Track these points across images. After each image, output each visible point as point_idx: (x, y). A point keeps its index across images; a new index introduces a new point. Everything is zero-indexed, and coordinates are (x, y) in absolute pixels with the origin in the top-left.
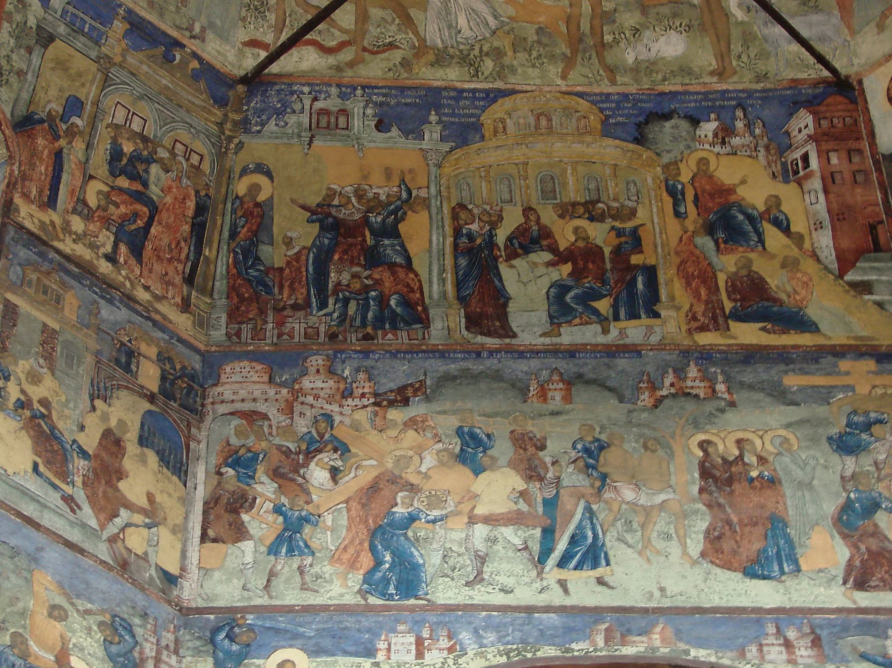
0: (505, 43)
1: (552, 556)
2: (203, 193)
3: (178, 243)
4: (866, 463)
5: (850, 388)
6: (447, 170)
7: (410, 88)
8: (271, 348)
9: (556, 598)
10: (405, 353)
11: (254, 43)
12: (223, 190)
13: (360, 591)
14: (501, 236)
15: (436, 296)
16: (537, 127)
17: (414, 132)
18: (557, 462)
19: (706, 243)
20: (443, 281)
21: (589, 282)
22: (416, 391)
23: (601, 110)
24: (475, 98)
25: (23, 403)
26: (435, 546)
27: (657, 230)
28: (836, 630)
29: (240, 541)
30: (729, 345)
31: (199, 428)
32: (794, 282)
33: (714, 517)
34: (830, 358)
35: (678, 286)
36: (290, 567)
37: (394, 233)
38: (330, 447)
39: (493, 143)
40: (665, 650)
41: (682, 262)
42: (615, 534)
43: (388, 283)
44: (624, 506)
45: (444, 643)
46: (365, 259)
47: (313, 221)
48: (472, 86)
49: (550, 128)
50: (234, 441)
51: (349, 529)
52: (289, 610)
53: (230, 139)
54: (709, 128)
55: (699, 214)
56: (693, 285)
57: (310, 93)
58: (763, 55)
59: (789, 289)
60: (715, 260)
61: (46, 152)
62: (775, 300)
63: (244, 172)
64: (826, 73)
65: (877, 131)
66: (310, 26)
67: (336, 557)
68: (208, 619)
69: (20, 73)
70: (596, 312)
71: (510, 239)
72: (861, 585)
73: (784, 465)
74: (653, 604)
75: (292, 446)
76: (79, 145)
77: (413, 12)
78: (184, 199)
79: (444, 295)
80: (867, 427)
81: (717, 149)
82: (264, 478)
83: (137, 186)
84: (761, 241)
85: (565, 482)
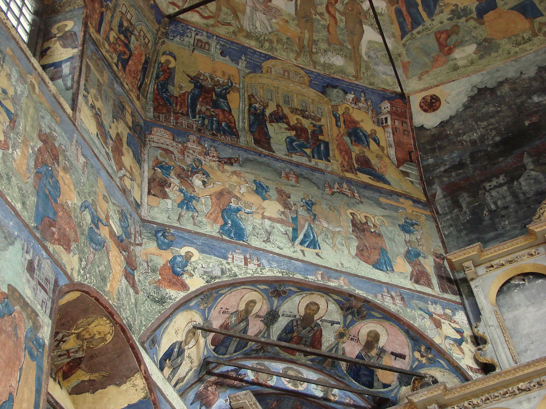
0: (274, 39)
1: (297, 240)
2: (147, 56)
3: (137, 72)
4: (413, 238)
5: (404, 209)
6: (247, 80)
7: (235, 43)
8: (173, 127)
9: (300, 256)
10: (230, 145)
12: (155, 58)
13: (219, 232)
14: (268, 112)
15: (241, 128)
16: (284, 75)
18: (295, 204)
19: (347, 139)
20: (244, 123)
21: (302, 141)
22: (236, 161)
23: (310, 77)
24: (260, 56)
25: (93, 106)
26: (249, 223)
27: (329, 129)
28: (409, 296)
29: (165, 198)
30: (358, 180)
31: (144, 149)
32: (381, 164)
33: (359, 242)
34: (396, 196)
35: (337, 153)
36: (188, 214)
38: (201, 172)
39: (265, 76)
40: (345, 287)
41: (339, 144)
42: (322, 238)
44: (324, 228)
45: (256, 262)
46: (212, 104)
47: (191, 82)
48: (260, 51)
49: (289, 77)
50: (159, 158)
51: (212, 206)
52: (189, 232)
53: (160, 38)
54: (351, 96)
55: (345, 128)
56: (343, 154)
57: (195, 31)
58: (372, 75)
59: (379, 166)
60: (351, 147)
61: (98, 10)
62: (374, 169)
63: (164, 53)
64: (399, 90)
65: (414, 117)
67: (208, 215)
68: (154, 226)
70: (305, 153)
71: (271, 115)
72: (417, 282)
73: (383, 230)
74: (339, 269)
77: (239, 14)
78: (141, 55)
80: (413, 225)
81: (353, 105)
82: (174, 177)
83: (126, 41)
84: (368, 145)
85: (300, 213)
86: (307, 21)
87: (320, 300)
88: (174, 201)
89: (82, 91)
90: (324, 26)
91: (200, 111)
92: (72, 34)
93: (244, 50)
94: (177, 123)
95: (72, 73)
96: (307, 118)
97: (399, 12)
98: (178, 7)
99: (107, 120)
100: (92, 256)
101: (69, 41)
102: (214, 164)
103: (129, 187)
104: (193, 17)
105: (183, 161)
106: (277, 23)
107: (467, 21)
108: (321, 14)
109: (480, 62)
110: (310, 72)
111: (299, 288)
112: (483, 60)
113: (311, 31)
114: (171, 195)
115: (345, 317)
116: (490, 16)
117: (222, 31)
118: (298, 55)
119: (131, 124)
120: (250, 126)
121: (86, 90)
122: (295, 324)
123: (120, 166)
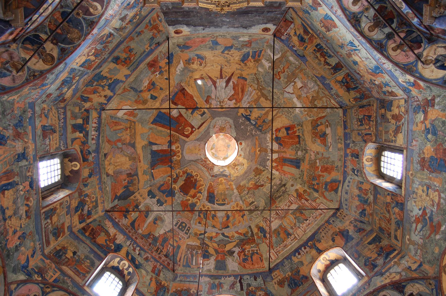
6: (329, 78)
14: (330, 67)
37: (342, 81)
54: (295, 49)
76: (363, 131)
84: (300, 34)
87: (366, 30)
90: (289, 69)
93: (323, 84)
100: (440, 132)
108: (287, 72)
111: (371, 42)
115: (360, 17)
120: (340, 70)
122: (382, 26)
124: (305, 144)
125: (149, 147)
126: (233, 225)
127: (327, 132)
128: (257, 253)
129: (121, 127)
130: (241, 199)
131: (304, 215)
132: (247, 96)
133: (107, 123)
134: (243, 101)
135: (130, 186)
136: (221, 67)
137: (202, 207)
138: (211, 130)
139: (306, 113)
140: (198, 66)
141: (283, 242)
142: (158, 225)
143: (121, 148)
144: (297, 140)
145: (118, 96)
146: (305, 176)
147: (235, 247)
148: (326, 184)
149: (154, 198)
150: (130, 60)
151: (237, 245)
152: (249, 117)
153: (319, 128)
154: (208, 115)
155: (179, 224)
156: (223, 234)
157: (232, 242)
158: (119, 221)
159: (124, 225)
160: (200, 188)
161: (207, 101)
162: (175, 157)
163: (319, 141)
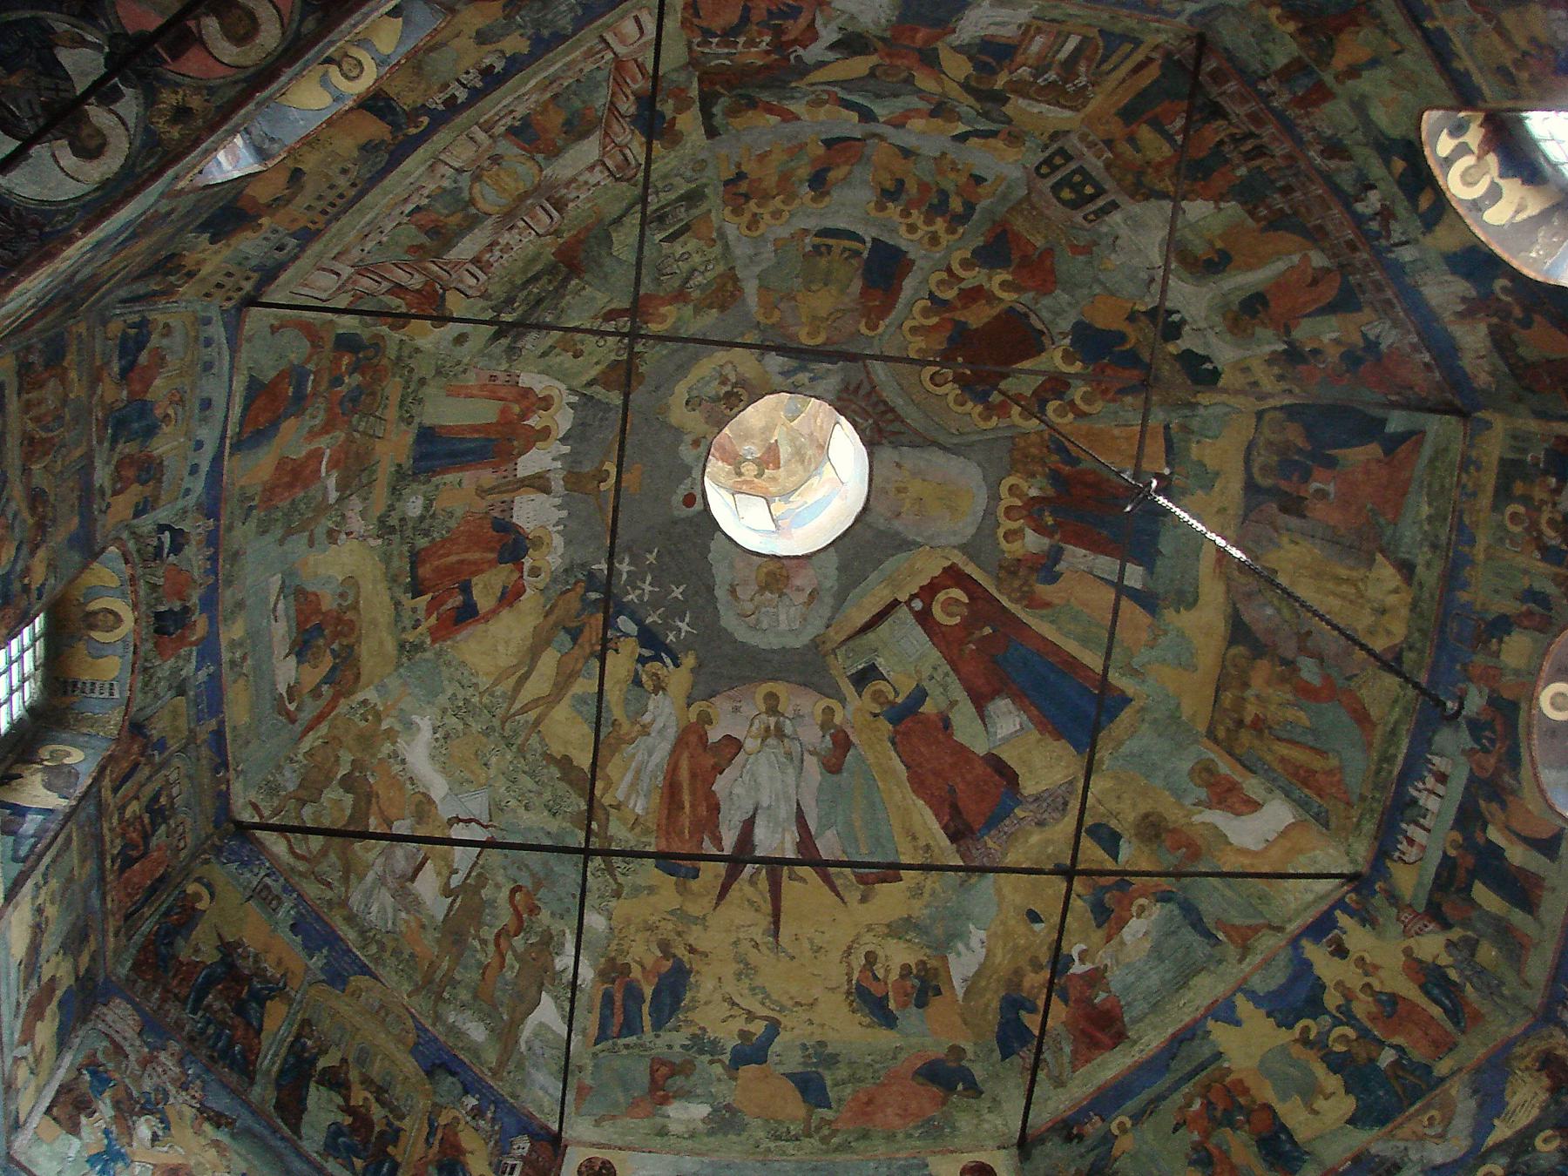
6: (312, 991)
11: (255, 807)
14: (322, 1063)
17: (310, 950)
43: (240, 1033)
50: (100, 1056)
53: (205, 852)
54: (471, 1101)
63: (199, 880)
64: (555, 1127)
66: (294, 829)
69: (157, 697)
75: (135, 1094)
77: (352, 876)
79: (269, 1071)
82: (108, 1101)
83: (148, 828)
86: (455, 943)
88: (85, 1146)
89: (37, 876)
90: (480, 963)
91: (210, 1006)
92: (72, 774)
93: (332, 939)
94: (160, 1008)
95: (38, 836)
96: (383, 1104)
97: (608, 999)
98: (261, 817)
99: (50, 944)
101: (60, 782)
102: (189, 1113)
103: (20, 1083)
104: (277, 845)
105: (138, 1080)
106: (407, 922)
107: (711, 1062)
108: (484, 942)
109: (706, 1140)
110: (420, 1028)
112: (712, 1139)
113: (457, 960)
114: (85, 1131)
116: (748, 1071)
117: (312, 890)
118: (417, 990)
119: (82, 973)
120: (282, 1072)
121: (45, 875)
123: (28, 1037)
124: (387, 558)
125: (1161, 590)
126: (802, 146)
127: (292, 660)
128: (707, 33)
129: (1283, 750)
130: (727, 246)
131: (420, 227)
132: (651, 766)
133: (1349, 804)
134: (672, 733)
135: (1300, 451)
136: (776, 934)
137: (945, 238)
138: (831, 582)
139: (384, 726)
140: (880, 953)
141: (556, 96)
142: (1211, 243)
143: (1302, 650)
144: (425, 571)
145: (1276, 922)
146: (395, 399)
147: (822, 64)
148: (300, 402)
149: (1188, 352)
150: (1209, 1105)
151: (803, 70)
152: (647, 653)
153: (327, 662)
154: (842, 667)
155: (1091, 207)
156: (867, 116)
157: (829, 83)
158: (1415, 348)
159: (1396, 324)
160: (935, 320)
161: (842, 743)
162: (1034, 493)
163: (329, 603)
